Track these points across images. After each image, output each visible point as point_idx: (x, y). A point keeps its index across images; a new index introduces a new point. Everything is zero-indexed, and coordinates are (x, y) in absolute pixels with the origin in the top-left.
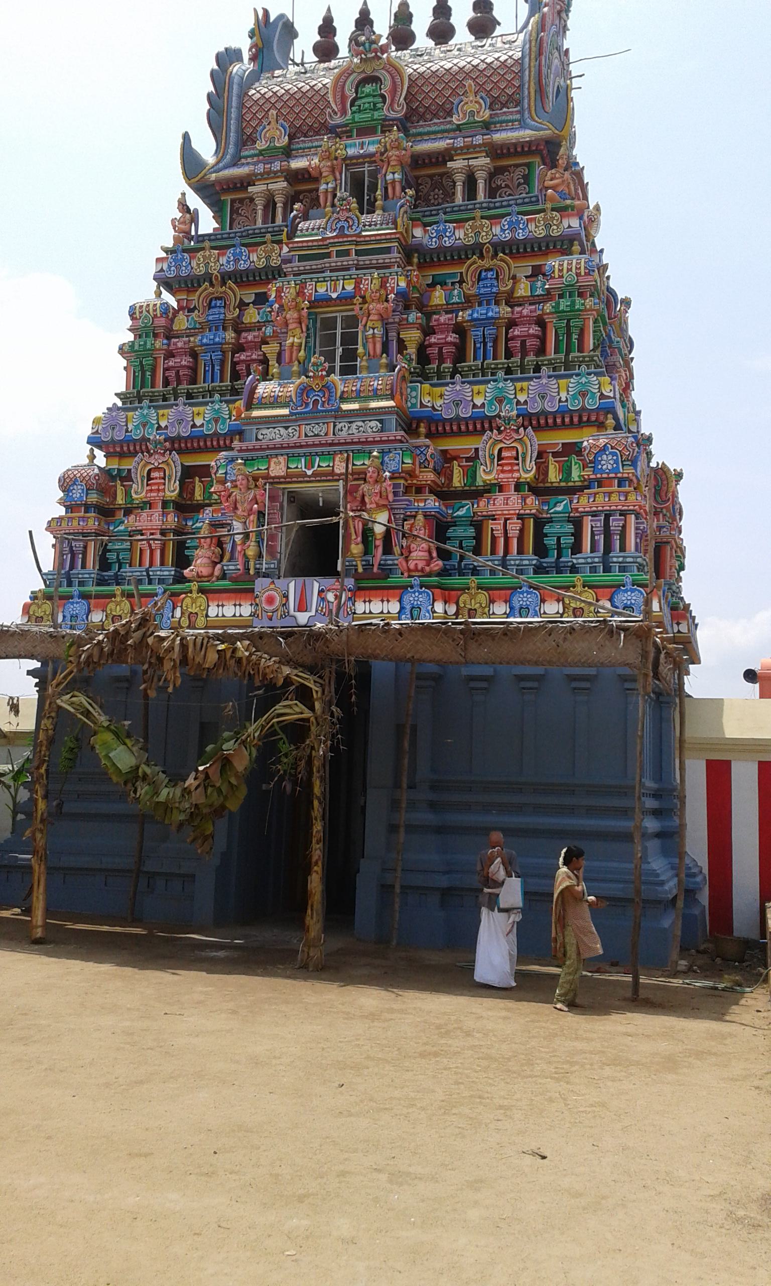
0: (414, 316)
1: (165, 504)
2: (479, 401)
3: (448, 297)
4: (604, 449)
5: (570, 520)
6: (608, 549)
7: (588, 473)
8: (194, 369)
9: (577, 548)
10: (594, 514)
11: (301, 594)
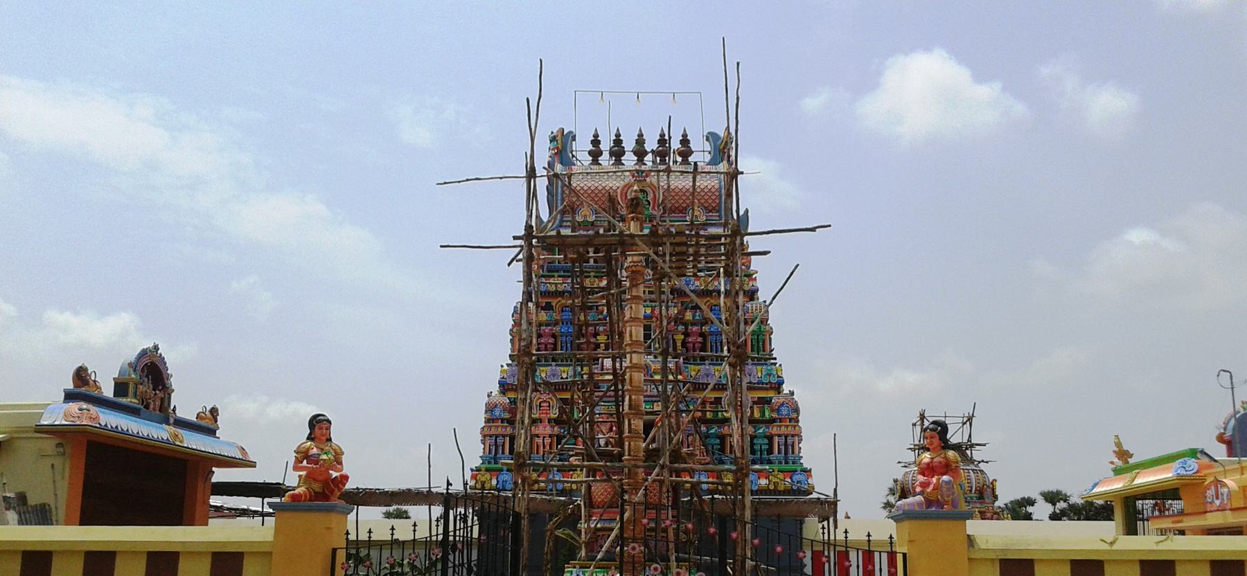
0: (681, 328)
1: (549, 421)
2: (564, 376)
3: (694, 316)
4: (782, 404)
5: (766, 437)
6: (786, 453)
7: (775, 415)
8: (555, 344)
9: (770, 451)
10: (779, 436)
11: (47, 432)
